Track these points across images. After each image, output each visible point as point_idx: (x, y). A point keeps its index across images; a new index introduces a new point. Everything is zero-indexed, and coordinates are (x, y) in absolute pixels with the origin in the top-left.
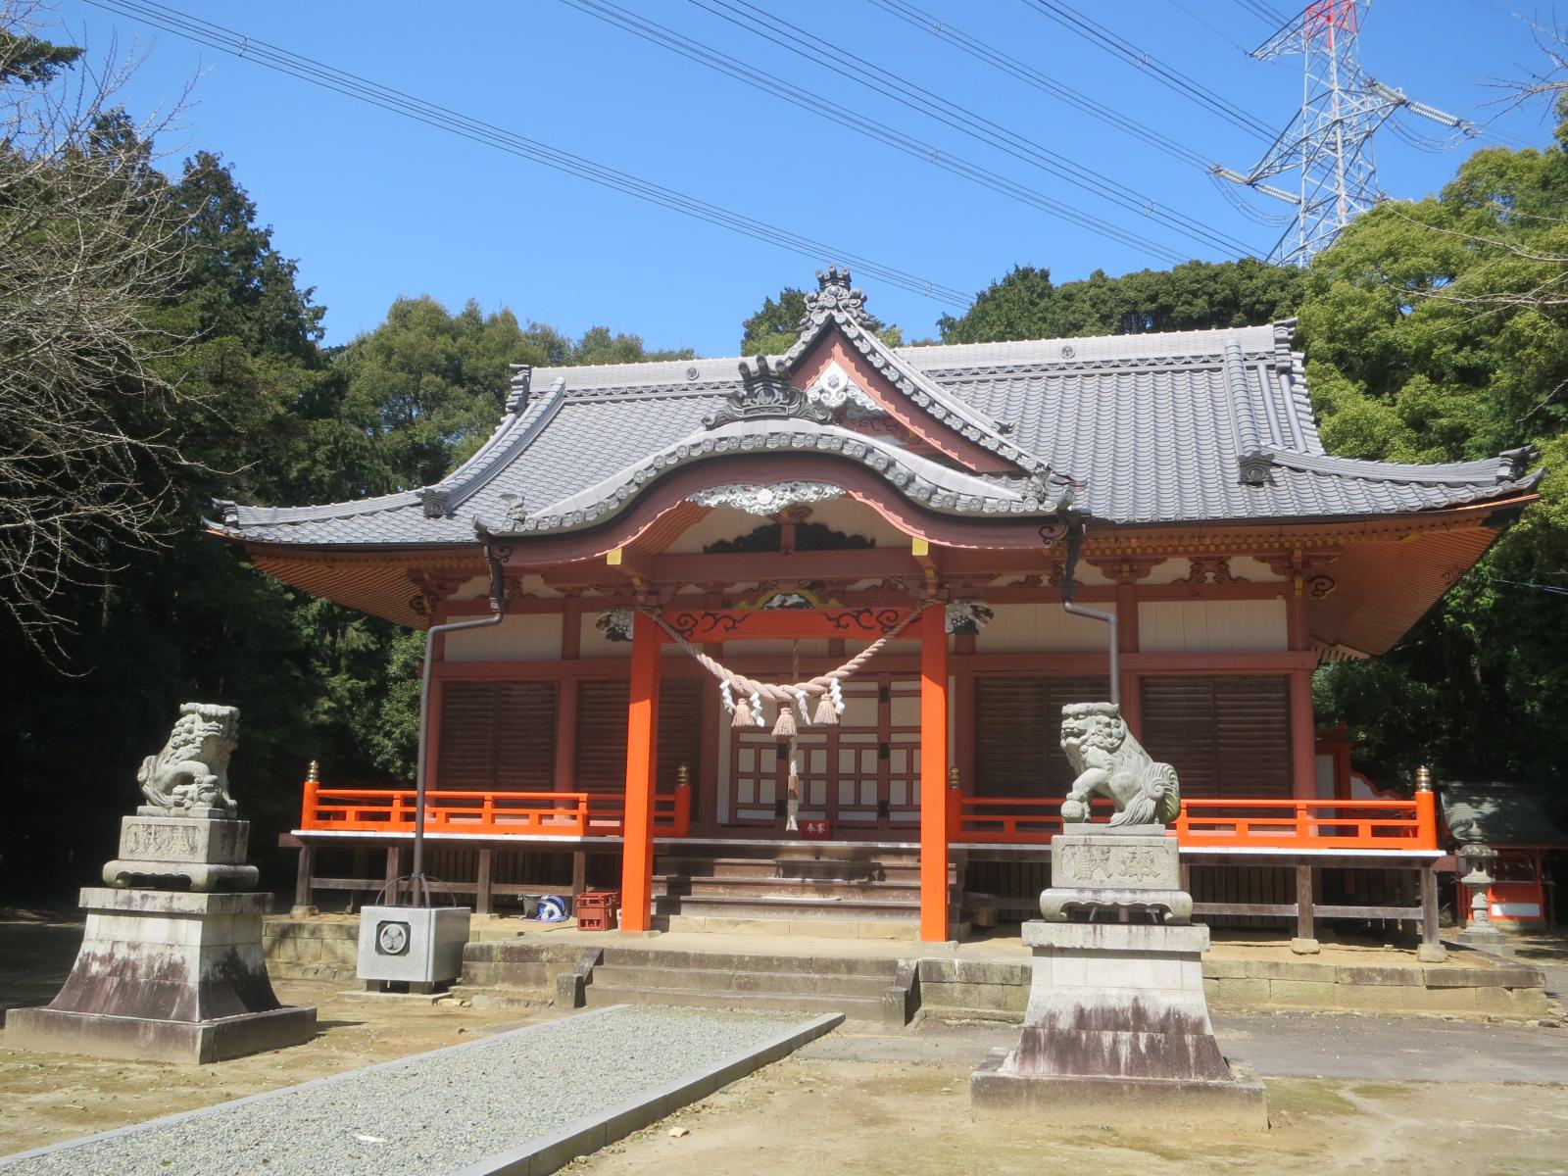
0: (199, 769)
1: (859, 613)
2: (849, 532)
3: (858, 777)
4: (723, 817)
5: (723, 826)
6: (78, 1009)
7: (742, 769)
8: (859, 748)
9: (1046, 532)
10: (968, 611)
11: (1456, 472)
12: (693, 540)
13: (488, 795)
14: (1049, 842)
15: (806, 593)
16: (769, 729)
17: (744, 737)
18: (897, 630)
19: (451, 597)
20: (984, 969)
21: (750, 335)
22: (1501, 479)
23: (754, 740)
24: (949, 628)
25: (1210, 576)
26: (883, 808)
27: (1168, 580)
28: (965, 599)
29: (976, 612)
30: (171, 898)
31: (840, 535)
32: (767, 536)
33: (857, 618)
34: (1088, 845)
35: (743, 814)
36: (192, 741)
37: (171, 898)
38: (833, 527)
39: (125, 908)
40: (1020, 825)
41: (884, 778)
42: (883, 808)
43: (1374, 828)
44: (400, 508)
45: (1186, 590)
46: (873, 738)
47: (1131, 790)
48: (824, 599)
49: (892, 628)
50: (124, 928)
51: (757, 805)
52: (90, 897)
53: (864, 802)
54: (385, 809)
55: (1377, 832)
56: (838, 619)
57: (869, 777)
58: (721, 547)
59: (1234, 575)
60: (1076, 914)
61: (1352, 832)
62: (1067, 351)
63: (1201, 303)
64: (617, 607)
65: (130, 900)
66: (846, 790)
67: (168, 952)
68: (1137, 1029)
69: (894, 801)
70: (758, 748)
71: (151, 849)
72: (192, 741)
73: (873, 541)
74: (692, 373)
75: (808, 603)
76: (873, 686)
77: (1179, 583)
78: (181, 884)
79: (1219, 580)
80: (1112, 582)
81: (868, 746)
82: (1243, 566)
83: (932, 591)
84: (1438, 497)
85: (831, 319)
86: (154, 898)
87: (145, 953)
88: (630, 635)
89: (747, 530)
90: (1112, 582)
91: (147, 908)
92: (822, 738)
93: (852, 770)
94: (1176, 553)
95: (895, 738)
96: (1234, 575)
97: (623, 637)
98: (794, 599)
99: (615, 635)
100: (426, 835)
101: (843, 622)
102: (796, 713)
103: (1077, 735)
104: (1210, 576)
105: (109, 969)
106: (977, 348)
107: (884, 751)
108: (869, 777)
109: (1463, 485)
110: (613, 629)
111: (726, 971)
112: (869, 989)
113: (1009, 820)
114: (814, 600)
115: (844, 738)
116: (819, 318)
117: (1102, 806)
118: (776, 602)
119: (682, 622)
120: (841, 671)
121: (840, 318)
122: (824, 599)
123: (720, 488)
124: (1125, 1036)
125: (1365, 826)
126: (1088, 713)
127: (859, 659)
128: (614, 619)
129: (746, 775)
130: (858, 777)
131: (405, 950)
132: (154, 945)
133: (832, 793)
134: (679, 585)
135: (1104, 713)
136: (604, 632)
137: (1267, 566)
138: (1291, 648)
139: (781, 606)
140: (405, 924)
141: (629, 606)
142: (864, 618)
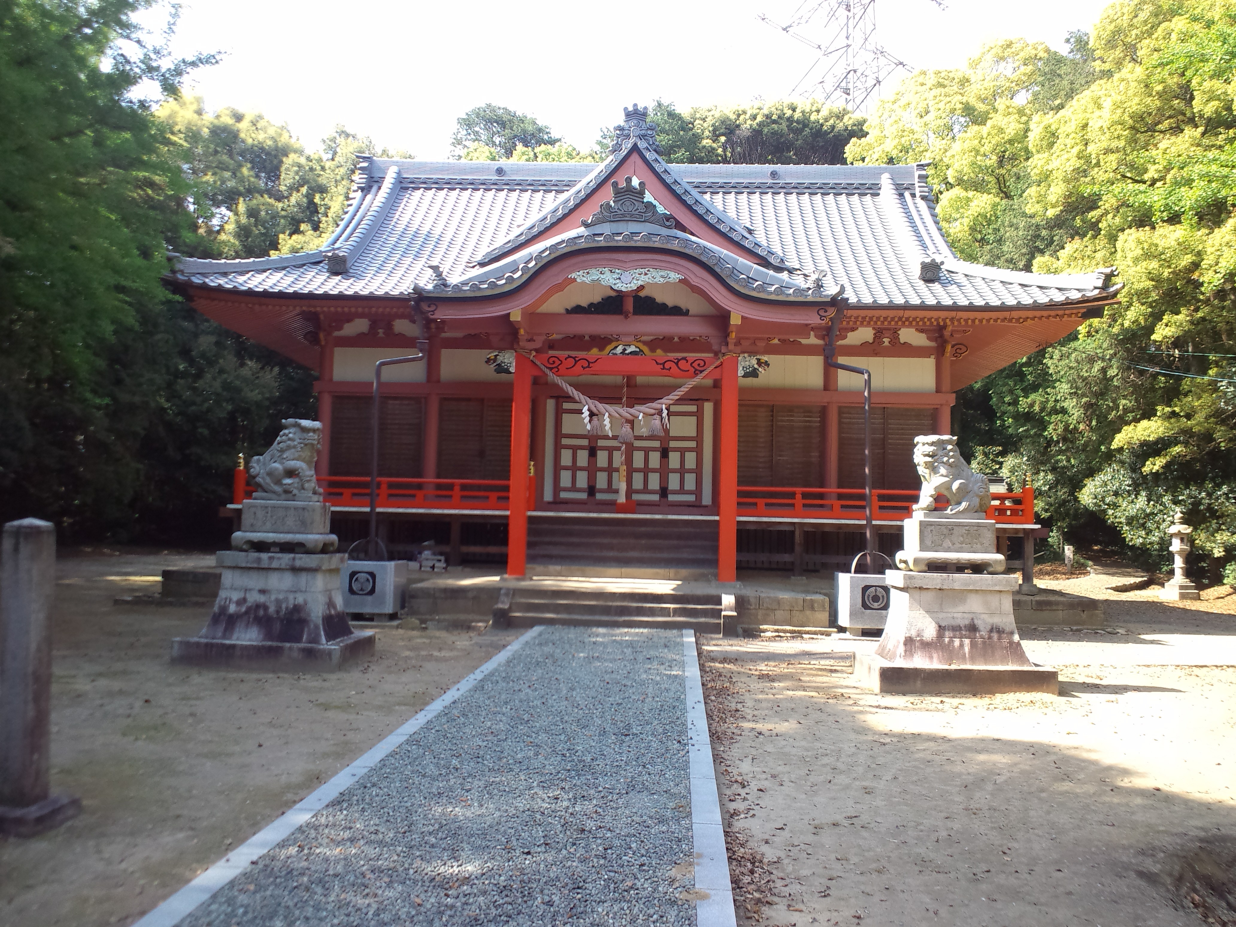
1: (679, 360)
2: (670, 303)
3: (574, 468)
4: (548, 496)
5: (549, 503)
6: (224, 637)
8: (647, 451)
9: (822, 313)
10: (754, 362)
12: (556, 304)
13: (799, 490)
18: (705, 373)
19: (337, 333)
21: (467, 123)
24: (741, 373)
25: (886, 341)
26: (592, 490)
27: (858, 342)
28: (752, 353)
29: (759, 363)
30: (294, 559)
31: (664, 305)
32: (613, 304)
33: (677, 364)
35: (563, 495)
37: (294, 559)
38: (659, 299)
39: (255, 565)
41: (592, 470)
42: (592, 490)
44: (304, 265)
45: (871, 349)
48: (653, 350)
49: (701, 372)
50: (254, 581)
51: (574, 488)
53: (686, 488)
54: (450, 493)
57: (654, 471)
58: (578, 310)
59: (902, 341)
62: (774, 174)
65: (259, 560)
66: (674, 482)
67: (291, 597)
69: (598, 486)
72: (294, 447)
73: (688, 311)
76: (693, 408)
77: (865, 344)
81: (654, 449)
86: (279, 558)
88: (512, 370)
89: (597, 298)
93: (678, 466)
95: (673, 444)
96: (902, 341)
98: (632, 349)
99: (501, 369)
100: (379, 510)
101: (667, 365)
104: (886, 341)
105: (243, 609)
108: (654, 471)
110: (499, 365)
113: (761, 502)
114: (645, 349)
118: (619, 349)
119: (551, 361)
122: (653, 350)
128: (500, 359)
129: (638, 470)
130: (646, 471)
131: (372, 592)
132: (279, 591)
133: (592, 479)
137: (923, 336)
138: (938, 390)
139: (623, 352)
142: (682, 364)
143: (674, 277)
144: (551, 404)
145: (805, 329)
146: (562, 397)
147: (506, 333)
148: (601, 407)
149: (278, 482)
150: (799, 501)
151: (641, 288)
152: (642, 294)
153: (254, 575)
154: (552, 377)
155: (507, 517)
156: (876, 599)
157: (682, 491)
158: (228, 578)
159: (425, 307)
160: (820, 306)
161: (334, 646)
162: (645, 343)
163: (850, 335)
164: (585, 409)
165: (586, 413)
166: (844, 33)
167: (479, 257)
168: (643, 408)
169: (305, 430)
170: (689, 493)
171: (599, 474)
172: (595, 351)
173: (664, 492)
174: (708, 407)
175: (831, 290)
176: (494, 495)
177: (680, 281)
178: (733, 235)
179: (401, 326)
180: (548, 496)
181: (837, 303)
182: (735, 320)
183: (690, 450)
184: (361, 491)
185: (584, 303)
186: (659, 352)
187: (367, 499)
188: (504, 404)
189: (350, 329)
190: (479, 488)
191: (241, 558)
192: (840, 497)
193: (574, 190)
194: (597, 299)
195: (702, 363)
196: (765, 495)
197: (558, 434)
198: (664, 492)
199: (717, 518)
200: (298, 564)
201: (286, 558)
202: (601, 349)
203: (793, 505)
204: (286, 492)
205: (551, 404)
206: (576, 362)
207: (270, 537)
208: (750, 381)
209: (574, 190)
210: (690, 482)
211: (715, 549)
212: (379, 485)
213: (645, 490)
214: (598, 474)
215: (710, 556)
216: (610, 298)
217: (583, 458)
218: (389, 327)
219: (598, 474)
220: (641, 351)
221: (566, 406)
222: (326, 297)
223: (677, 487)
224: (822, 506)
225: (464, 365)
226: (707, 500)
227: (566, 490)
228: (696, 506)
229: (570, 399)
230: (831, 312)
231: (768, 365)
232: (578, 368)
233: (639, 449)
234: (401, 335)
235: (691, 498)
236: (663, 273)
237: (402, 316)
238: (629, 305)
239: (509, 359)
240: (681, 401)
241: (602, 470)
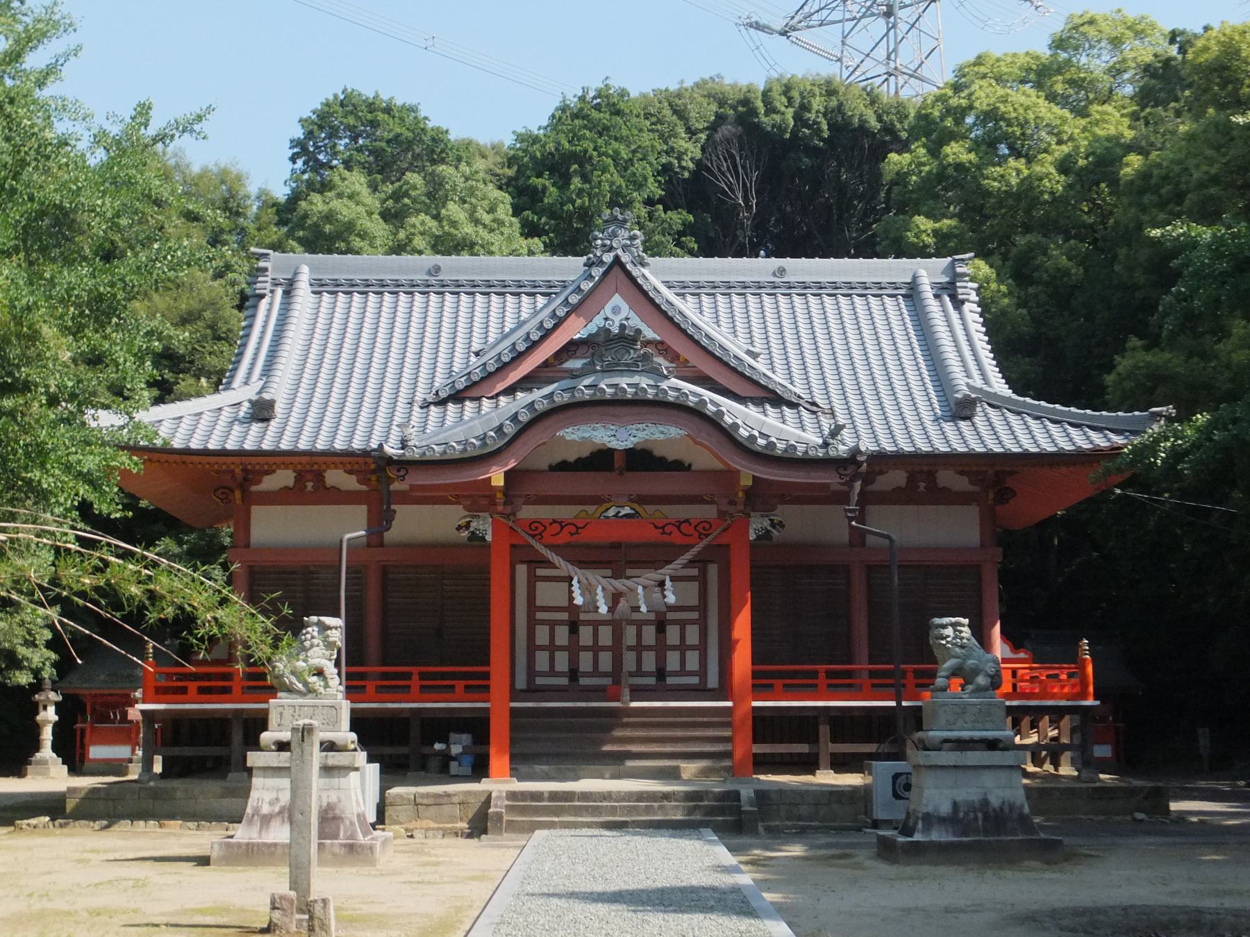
2: (671, 457)
5: (522, 691)
8: (683, 624)
10: (766, 523)
13: (415, 670)
14: (267, 702)
15: (636, 506)
23: (710, 620)
25: (310, 485)
29: (773, 525)
31: (662, 460)
32: (601, 460)
35: (540, 681)
38: (658, 452)
43: (467, 687)
46: (565, 616)
49: (707, 536)
51: (552, 672)
52: (254, 759)
54: (814, 682)
55: (202, 690)
56: (663, 528)
57: (649, 648)
58: (563, 466)
61: (183, 691)
66: (629, 661)
69: (669, 668)
73: (690, 465)
77: (287, 488)
79: (316, 488)
80: (364, 488)
81: (561, 623)
89: (585, 453)
90: (364, 488)
98: (627, 510)
100: (904, 704)
101: (667, 529)
104: (310, 485)
105: (277, 809)
107: (574, 627)
108: (649, 648)
110: (473, 533)
115: (670, 616)
118: (611, 513)
125: (193, 686)
129: (542, 648)
139: (616, 515)
144: (522, 570)
146: (537, 562)
155: (487, 709)
163: (266, 479)
173: (574, 674)
174: (713, 570)
180: (521, 683)
183: (692, 622)
184: (393, 685)
185: (572, 459)
187: (892, 690)
188: (483, 573)
189: (271, 483)
190: (443, 676)
192: (872, 674)
195: (707, 526)
197: (532, 607)
198: (574, 674)
199: (729, 704)
203: (815, 686)
205: (522, 570)
206: (562, 528)
207: (966, 734)
212: (905, 672)
214: (669, 653)
215: (803, 748)
217: (562, 636)
218: (319, 477)
219: (669, 653)
220: (637, 512)
221: (541, 572)
224: (850, 685)
225: (415, 523)
226: (713, 681)
228: (701, 691)
229: (549, 564)
230: (851, 470)
231: (783, 526)
233: (674, 622)
234: (335, 489)
235: (695, 680)
236: (661, 428)
238: (618, 462)
241: (586, 648)
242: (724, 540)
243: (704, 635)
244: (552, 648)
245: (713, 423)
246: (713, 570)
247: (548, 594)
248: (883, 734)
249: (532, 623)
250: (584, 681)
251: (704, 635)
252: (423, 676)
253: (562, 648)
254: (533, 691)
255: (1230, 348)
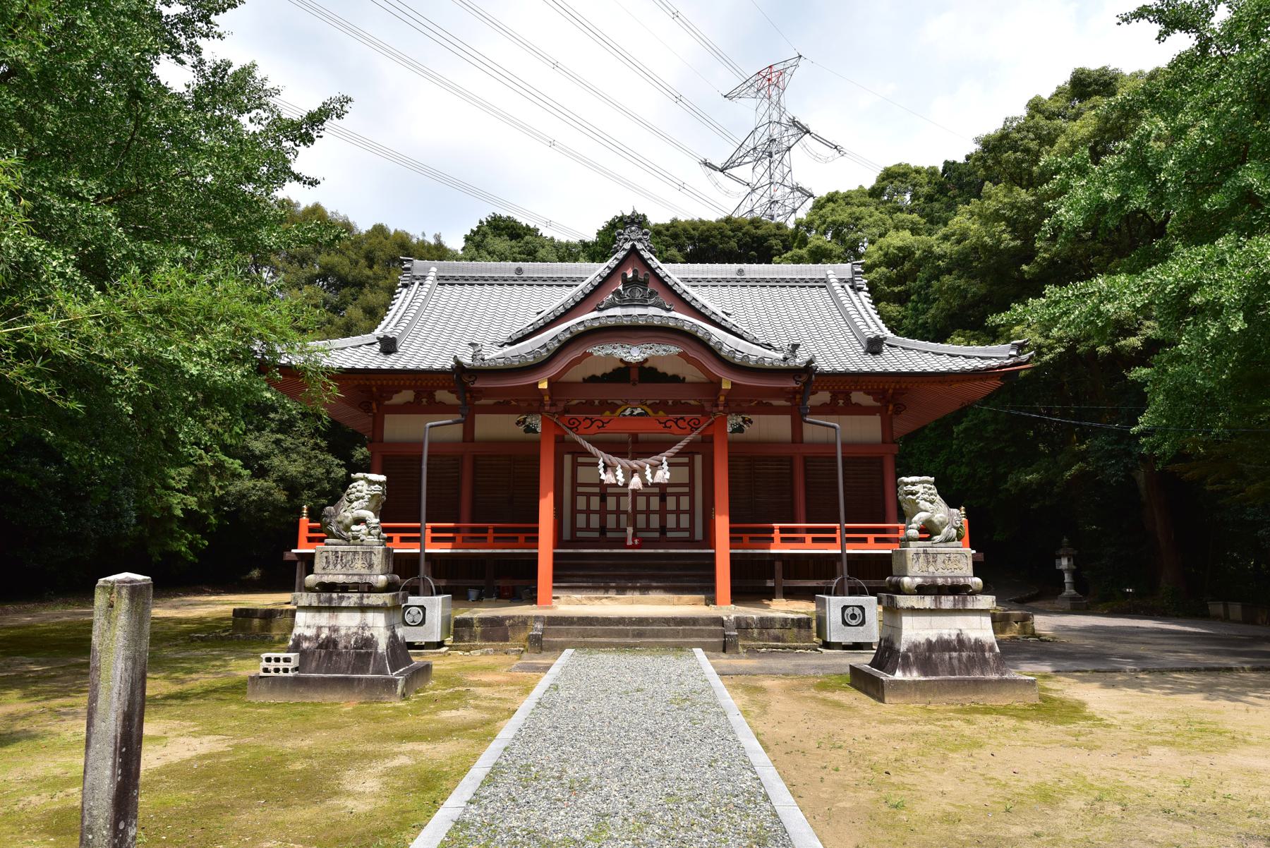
0: (369, 515)
2: (670, 372)
7: (579, 507)
8: (678, 495)
10: (740, 420)
11: (985, 351)
12: (577, 374)
13: (490, 525)
16: (626, 485)
17: (610, 490)
20: (772, 620)
22: (1011, 356)
24: (729, 429)
25: (841, 402)
26: (603, 529)
28: (738, 413)
31: (665, 374)
32: (624, 373)
34: (925, 552)
35: (579, 534)
36: (363, 498)
38: (661, 369)
40: (751, 539)
47: (943, 524)
50: (324, 619)
51: (588, 529)
57: (654, 512)
58: (593, 379)
60: (921, 590)
63: (733, 244)
64: (530, 412)
65: (331, 599)
66: (671, 521)
68: (960, 650)
69: (669, 526)
70: (618, 496)
71: (339, 566)
72: (363, 498)
74: (519, 270)
75: (646, 414)
76: (686, 460)
77: (824, 405)
78: (371, 589)
81: (594, 494)
82: (858, 397)
83: (721, 408)
84: (981, 364)
85: (633, 246)
87: (343, 632)
88: (539, 430)
90: (789, 404)
91: (344, 604)
92: (657, 490)
94: (823, 390)
97: (535, 431)
99: (529, 429)
100: (427, 551)
102: (643, 477)
103: (913, 494)
104: (841, 402)
106: (698, 266)
107: (603, 497)
108: (654, 512)
109: (990, 358)
111: (621, 627)
112: (712, 634)
114: (649, 411)
115: (669, 490)
116: (628, 246)
117: (928, 530)
118: (628, 412)
120: (668, 453)
121: (639, 246)
122: (655, 412)
123: (606, 343)
124: (955, 654)
126: (921, 482)
127: (682, 444)
128: (529, 420)
129: (581, 512)
130: (648, 512)
131: (422, 623)
133: (603, 521)
134: (568, 401)
135: (928, 482)
136: (522, 428)
138: (884, 442)
140: (422, 607)
141: (538, 412)
142: (681, 423)
143: (674, 350)
144: (568, 459)
145: (780, 393)
147: (527, 402)
148: (615, 460)
149: (347, 528)
150: (490, 535)
151: (646, 360)
152: (647, 365)
153: (326, 615)
154: (572, 435)
156: (853, 616)
157: (678, 529)
158: (301, 617)
159: (466, 379)
160: (794, 372)
161: (399, 676)
162: (649, 406)
163: (395, 396)
164: (601, 462)
165: (602, 465)
166: (767, 175)
167: (503, 337)
168: (649, 460)
169: (371, 483)
170: (684, 530)
171: (669, 516)
172: (608, 413)
174: (698, 459)
175: (800, 360)
176: (521, 537)
177: (680, 354)
178: (713, 317)
179: (443, 396)
180: (567, 535)
181: (809, 369)
182: (726, 386)
183: (684, 494)
185: (599, 373)
186: (661, 413)
191: (306, 599)
193: (582, 285)
194: (609, 370)
196: (809, 531)
197: (575, 484)
198: (663, 529)
200: (365, 601)
201: (353, 599)
202: (613, 411)
204: (355, 538)
205: (568, 459)
208: (737, 435)
209: (582, 285)
210: (685, 521)
211: (713, 578)
213: (588, 528)
216: (619, 369)
217: (595, 503)
218: (431, 396)
221: (580, 460)
222: (379, 371)
223: (674, 526)
225: (496, 426)
226: (699, 535)
227: (581, 530)
228: (690, 542)
230: (804, 378)
232: (594, 427)
233: (672, 494)
235: (687, 534)
237: (443, 388)
238: (634, 374)
239: (536, 421)
240: (677, 455)
241: (611, 512)
242: (709, 433)
243: (574, 502)
244: (588, 512)
245: (703, 344)
246: (698, 459)
247: (584, 475)
248: (876, 576)
249: (574, 494)
250: (609, 535)
251: (574, 502)
252: (496, 530)
253: (595, 512)
254: (575, 542)
255: (1090, 243)
